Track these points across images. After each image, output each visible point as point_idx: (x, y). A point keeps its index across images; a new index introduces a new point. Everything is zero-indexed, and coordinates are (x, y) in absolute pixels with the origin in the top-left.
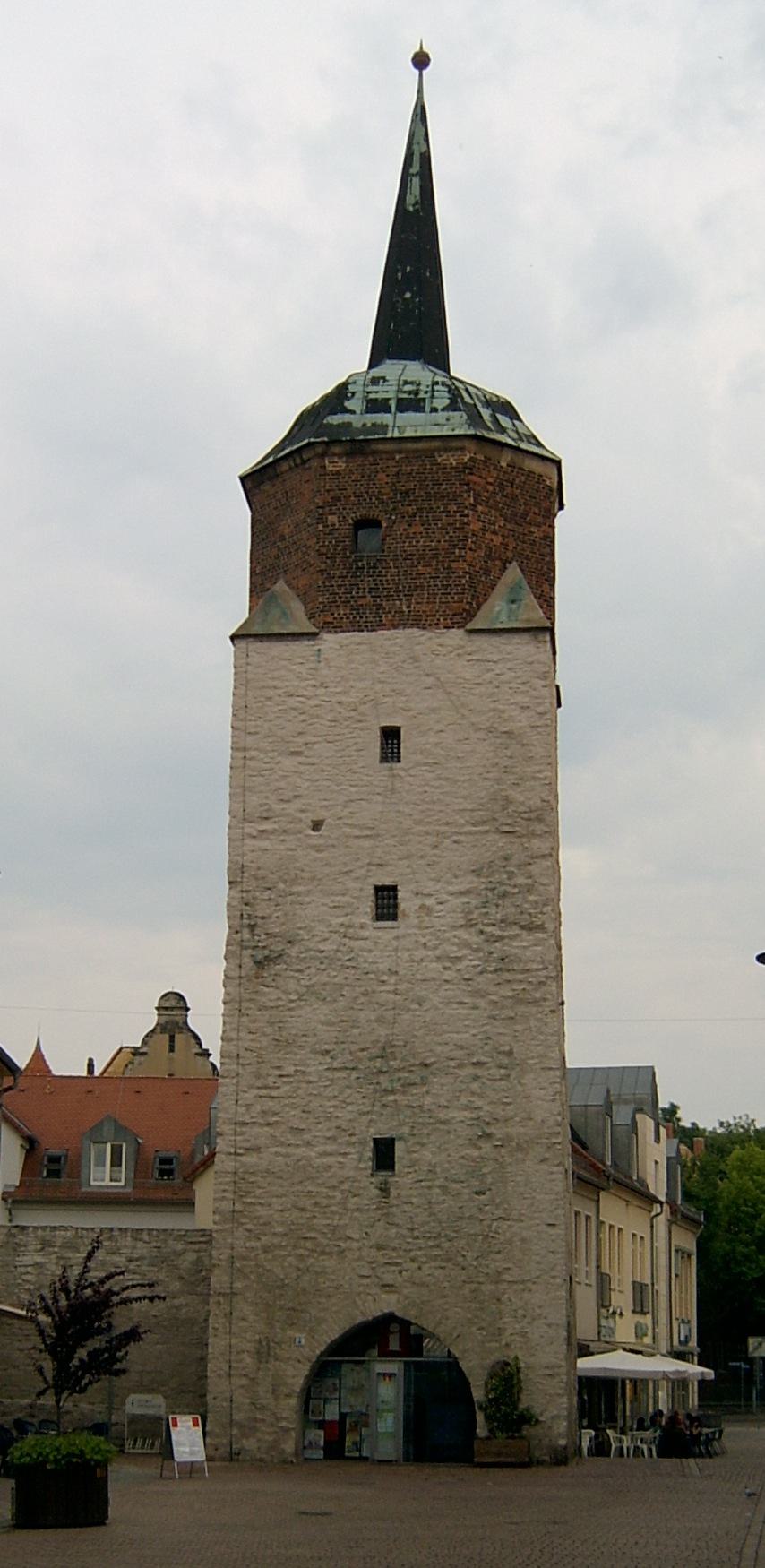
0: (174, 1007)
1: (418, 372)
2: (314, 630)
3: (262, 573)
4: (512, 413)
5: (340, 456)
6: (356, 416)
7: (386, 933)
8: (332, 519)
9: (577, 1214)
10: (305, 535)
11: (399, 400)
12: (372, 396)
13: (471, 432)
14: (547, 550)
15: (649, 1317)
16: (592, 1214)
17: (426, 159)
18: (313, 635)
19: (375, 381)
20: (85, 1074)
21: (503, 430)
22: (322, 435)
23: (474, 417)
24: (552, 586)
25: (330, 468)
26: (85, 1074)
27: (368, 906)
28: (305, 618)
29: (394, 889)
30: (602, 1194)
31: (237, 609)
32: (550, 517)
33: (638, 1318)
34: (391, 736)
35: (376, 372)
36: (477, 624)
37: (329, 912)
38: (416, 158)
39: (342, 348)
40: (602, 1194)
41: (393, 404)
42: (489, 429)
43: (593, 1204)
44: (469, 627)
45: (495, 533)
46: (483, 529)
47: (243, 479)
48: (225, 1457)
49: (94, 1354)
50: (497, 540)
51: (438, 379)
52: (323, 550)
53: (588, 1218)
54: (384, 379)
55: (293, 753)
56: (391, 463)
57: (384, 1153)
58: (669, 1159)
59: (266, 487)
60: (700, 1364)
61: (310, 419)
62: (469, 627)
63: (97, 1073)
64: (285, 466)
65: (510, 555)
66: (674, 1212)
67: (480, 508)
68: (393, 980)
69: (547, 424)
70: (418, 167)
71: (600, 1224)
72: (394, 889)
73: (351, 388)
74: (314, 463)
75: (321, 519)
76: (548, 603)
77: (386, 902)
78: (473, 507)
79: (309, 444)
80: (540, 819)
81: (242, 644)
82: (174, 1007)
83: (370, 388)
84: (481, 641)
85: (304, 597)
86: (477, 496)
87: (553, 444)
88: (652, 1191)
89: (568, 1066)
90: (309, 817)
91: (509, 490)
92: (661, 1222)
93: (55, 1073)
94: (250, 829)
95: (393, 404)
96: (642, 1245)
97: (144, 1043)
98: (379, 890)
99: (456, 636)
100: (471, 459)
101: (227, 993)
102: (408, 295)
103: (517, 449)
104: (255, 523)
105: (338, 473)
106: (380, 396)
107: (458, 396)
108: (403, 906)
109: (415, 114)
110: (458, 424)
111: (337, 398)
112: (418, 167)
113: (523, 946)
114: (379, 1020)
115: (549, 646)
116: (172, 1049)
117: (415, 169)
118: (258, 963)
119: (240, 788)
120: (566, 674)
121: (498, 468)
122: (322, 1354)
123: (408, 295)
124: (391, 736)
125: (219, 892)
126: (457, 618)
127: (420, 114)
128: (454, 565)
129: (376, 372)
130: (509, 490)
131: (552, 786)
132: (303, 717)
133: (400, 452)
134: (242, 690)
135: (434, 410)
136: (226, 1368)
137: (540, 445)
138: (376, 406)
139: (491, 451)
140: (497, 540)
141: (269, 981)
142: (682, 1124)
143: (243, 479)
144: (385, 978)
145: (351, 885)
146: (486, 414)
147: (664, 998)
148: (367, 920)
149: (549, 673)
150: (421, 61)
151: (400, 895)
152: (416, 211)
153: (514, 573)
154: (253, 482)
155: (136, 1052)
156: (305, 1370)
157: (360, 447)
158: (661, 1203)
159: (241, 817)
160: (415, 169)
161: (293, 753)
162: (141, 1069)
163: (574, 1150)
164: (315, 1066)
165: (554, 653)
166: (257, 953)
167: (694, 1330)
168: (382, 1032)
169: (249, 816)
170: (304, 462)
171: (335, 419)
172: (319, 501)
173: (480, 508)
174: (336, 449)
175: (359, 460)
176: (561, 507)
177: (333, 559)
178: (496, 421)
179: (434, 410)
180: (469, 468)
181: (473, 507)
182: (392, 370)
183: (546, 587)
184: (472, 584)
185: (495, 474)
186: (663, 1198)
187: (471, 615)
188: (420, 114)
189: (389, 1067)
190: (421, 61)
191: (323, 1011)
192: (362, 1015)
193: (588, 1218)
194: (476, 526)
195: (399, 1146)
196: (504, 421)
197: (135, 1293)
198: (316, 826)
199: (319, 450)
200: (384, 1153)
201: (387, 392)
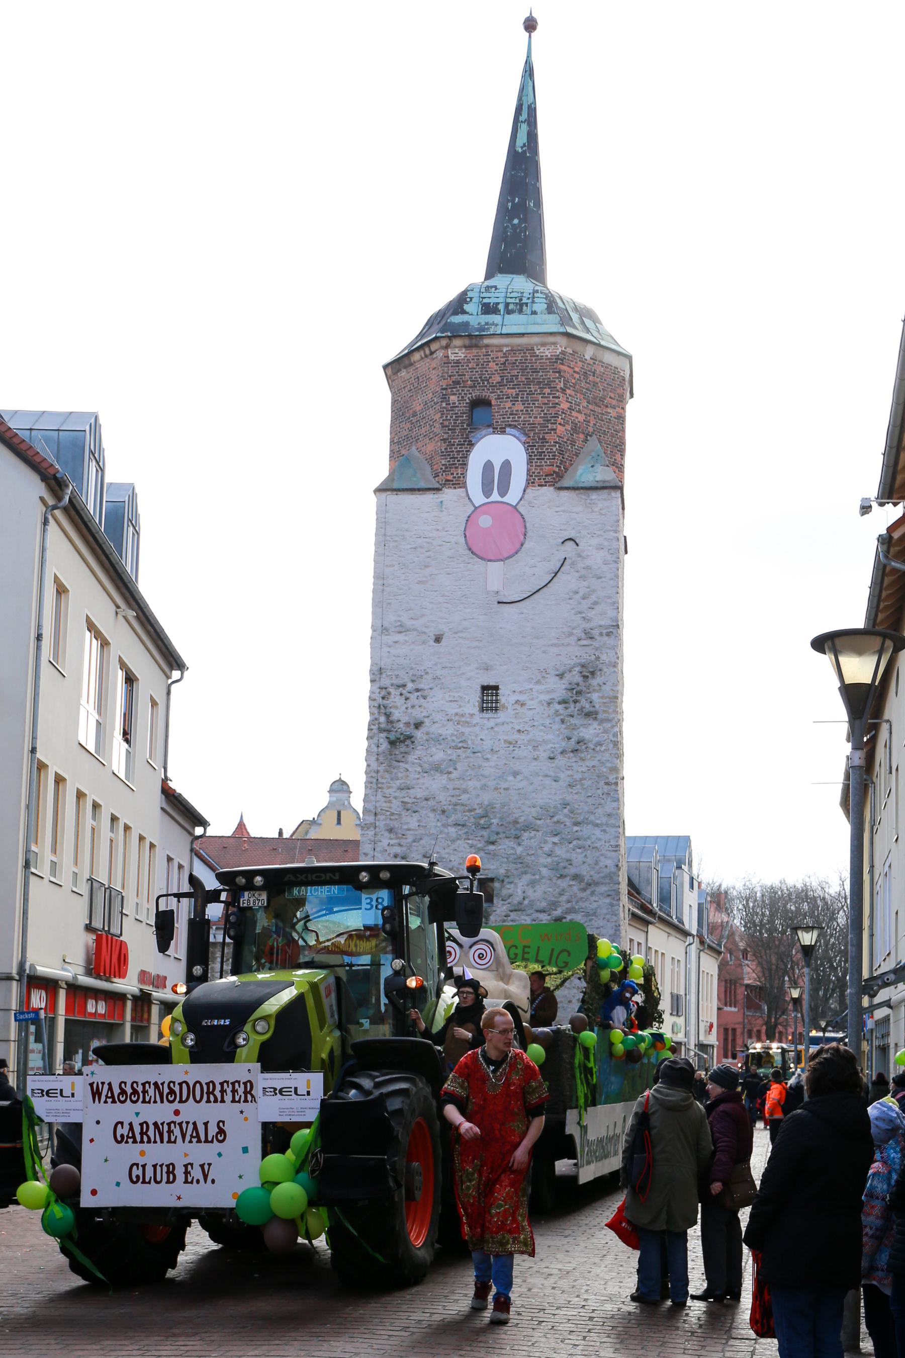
0: (340, 787)
1: (521, 284)
2: (437, 486)
3: (399, 443)
4: (595, 320)
5: (460, 347)
6: (473, 317)
8: (453, 398)
10: (432, 411)
11: (507, 305)
12: (485, 301)
13: (562, 330)
15: (682, 1019)
16: (643, 941)
17: (532, 111)
18: (438, 490)
19: (488, 288)
20: (277, 836)
21: (588, 330)
22: (449, 326)
24: (623, 456)
25: (452, 357)
26: (277, 836)
27: (475, 696)
28: (431, 478)
29: (496, 688)
31: (381, 470)
32: (621, 401)
33: (675, 1019)
34: (490, 691)
35: (489, 283)
36: (566, 483)
37: (447, 705)
39: (464, 263)
40: (650, 926)
42: (575, 327)
43: (644, 934)
44: (557, 485)
45: (579, 412)
47: (385, 367)
49: (394, 919)
50: (581, 418)
51: (539, 288)
52: (446, 423)
53: (639, 944)
56: (500, 354)
59: (403, 373)
60: (21, 1138)
62: (557, 485)
64: (417, 356)
65: (591, 429)
66: (702, 942)
70: (526, 115)
72: (496, 688)
73: (470, 294)
74: (440, 354)
75: (444, 398)
76: (619, 468)
78: (563, 391)
79: (436, 338)
80: (609, 634)
81: (383, 495)
82: (340, 787)
86: (566, 382)
87: (626, 344)
90: (432, 632)
91: (591, 378)
93: (253, 834)
95: (501, 307)
96: (679, 966)
97: (319, 815)
98: (484, 688)
99: (548, 491)
100: (563, 353)
101: (368, 766)
102: (516, 221)
103: (599, 345)
104: (394, 402)
105: (458, 362)
106: (492, 301)
107: (552, 305)
108: (503, 699)
110: (551, 324)
111: (459, 304)
112: (526, 115)
113: (591, 731)
114: (484, 787)
115: (620, 500)
116: (339, 822)
117: (524, 116)
118: (392, 743)
119: (381, 602)
120: (631, 527)
121: (583, 361)
124: (490, 691)
126: (549, 478)
127: (529, 71)
128: (547, 437)
129: (489, 283)
130: (591, 378)
131: (617, 606)
134: (396, 448)
135: (534, 313)
137: (619, 345)
138: (488, 309)
139: (578, 346)
140: (581, 418)
141: (400, 757)
143: (687, 839)
146: (575, 317)
148: (476, 710)
149: (617, 525)
150: (530, 25)
152: (524, 152)
153: (594, 444)
154: (394, 368)
155: (313, 822)
157: (473, 339)
158: (694, 936)
159: (380, 630)
160: (524, 116)
162: (314, 834)
163: (629, 893)
164: (432, 821)
165: (623, 508)
166: (393, 739)
167: (806, 992)
168: (486, 798)
170: (432, 353)
171: (458, 319)
173: (568, 392)
176: (632, 396)
177: (453, 430)
178: (583, 323)
179: (534, 313)
180: (559, 359)
181: (563, 391)
182: (501, 281)
183: (618, 456)
184: (561, 452)
185: (580, 364)
186: (694, 932)
187: (560, 476)
188: (529, 71)
190: (530, 25)
191: (442, 780)
193: (639, 944)
194: (565, 406)
195: (460, 491)
196: (588, 322)
198: (438, 640)
199: (444, 342)
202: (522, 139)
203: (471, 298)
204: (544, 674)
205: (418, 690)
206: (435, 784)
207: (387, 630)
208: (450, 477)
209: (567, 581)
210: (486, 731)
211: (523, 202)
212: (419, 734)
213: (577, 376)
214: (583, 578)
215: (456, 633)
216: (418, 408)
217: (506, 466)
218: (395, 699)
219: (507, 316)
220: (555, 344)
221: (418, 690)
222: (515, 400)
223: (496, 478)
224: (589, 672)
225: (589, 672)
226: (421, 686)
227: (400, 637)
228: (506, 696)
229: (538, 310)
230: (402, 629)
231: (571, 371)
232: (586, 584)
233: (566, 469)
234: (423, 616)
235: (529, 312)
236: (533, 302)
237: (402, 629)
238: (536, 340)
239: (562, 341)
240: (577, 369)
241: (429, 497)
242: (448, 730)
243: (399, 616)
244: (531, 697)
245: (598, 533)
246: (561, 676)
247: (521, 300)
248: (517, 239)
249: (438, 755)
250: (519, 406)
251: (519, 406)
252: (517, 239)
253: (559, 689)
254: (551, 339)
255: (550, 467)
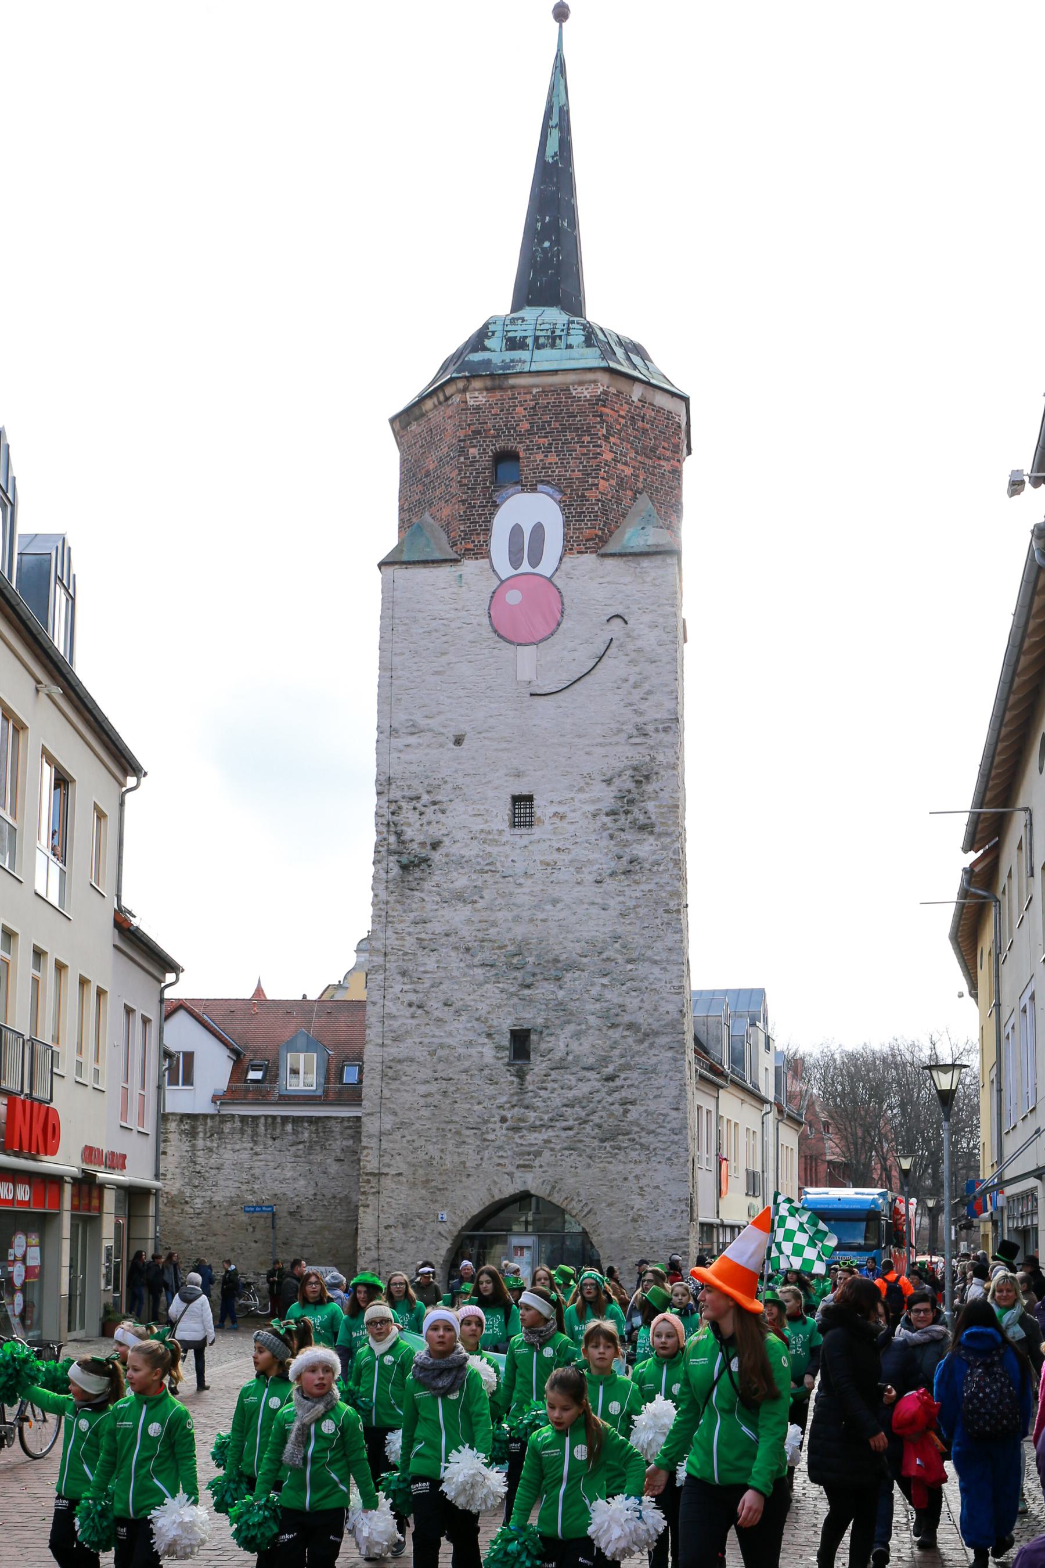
1: (555, 316)
2: (455, 556)
3: (410, 509)
5: (480, 390)
6: (496, 353)
7: (522, 837)
8: (473, 451)
9: (747, 1129)
10: (448, 469)
11: (537, 338)
12: (510, 335)
13: (603, 364)
14: (803, 1147)
16: (713, 1109)
17: (564, 115)
18: (456, 561)
21: (635, 367)
23: (607, 352)
27: (504, 809)
28: (448, 547)
30: (721, 1091)
31: (387, 537)
34: (522, 802)
35: (514, 315)
36: (611, 548)
37: (471, 821)
38: (556, 111)
39: (489, 288)
40: (721, 1091)
41: (530, 341)
43: (713, 1101)
45: (626, 464)
46: (615, 460)
47: (762, 992)
48: (545, 251)
50: (628, 471)
52: (465, 481)
53: (708, 1112)
54: (523, 320)
55: (436, 673)
56: (529, 397)
57: (521, 1043)
58: (776, 1068)
61: (457, 360)
63: (698, 1466)
65: (640, 485)
66: (780, 1111)
67: (612, 439)
68: (529, 882)
69: (671, 363)
70: (557, 121)
71: (719, 1118)
73: (491, 328)
74: (457, 399)
75: (462, 451)
77: (522, 804)
81: (390, 570)
83: (509, 328)
84: (609, 562)
85: (447, 527)
86: (609, 427)
88: (763, 1094)
89: (692, 989)
90: (451, 732)
91: (640, 424)
92: (771, 1118)
94: (399, 742)
95: (530, 341)
98: (516, 799)
99: (590, 559)
100: (605, 393)
101: (376, 896)
102: (547, 244)
103: (649, 384)
104: (403, 462)
105: (478, 408)
106: (519, 334)
107: (590, 336)
108: (538, 812)
109: (555, 67)
110: (591, 358)
112: (557, 121)
113: (645, 848)
114: (517, 919)
118: (404, 868)
122: (463, 1229)
123: (547, 244)
124: (522, 802)
125: (369, 802)
126: (591, 544)
127: (560, 67)
128: (587, 493)
130: (640, 424)
131: (675, 696)
132: (445, 639)
133: (537, 386)
135: (569, 347)
136: (374, 1240)
138: (514, 344)
139: (623, 385)
140: (628, 471)
141: (414, 885)
142: (444, 1488)
143: (762, 992)
144: (521, 881)
145: (490, 794)
146: (619, 352)
147: (820, 919)
148: (505, 826)
150: (561, 13)
151: (535, 802)
152: (556, 163)
154: (404, 421)
156: (446, 1245)
157: (497, 379)
161: (436, 673)
162: (340, 996)
164: (455, 961)
168: (519, 931)
169: (398, 725)
170: (447, 399)
172: (461, 434)
173: (612, 439)
174: (477, 384)
175: (498, 394)
177: (473, 489)
178: (629, 359)
179: (569, 347)
180: (602, 400)
181: (606, 438)
182: (530, 313)
184: (605, 512)
185: (626, 407)
186: (772, 1100)
187: (603, 541)
188: (560, 67)
189: (523, 965)
190: (561, 13)
192: (500, 914)
193: (708, 1112)
194: (608, 456)
197: (6, 1558)
198: (458, 741)
199: (461, 384)
200: (521, 1043)
201: (523, 331)
202: (553, 146)
203: (493, 333)
204: (588, 780)
205: (434, 803)
206: (458, 916)
207: (396, 731)
208: (471, 546)
209: (614, 667)
210: (517, 850)
211: (555, 221)
212: (437, 856)
213: (623, 421)
214: (633, 662)
215: (480, 733)
216: (431, 467)
217: (538, 530)
218: (407, 815)
219: (536, 352)
220: (595, 382)
221: (434, 803)
222: (547, 451)
223: (527, 545)
224: (642, 776)
225: (642, 776)
226: (439, 798)
227: (412, 740)
228: (542, 808)
229: (574, 344)
230: (415, 730)
231: (615, 415)
232: (637, 669)
233: (611, 533)
234: (439, 713)
235: (563, 346)
236: (568, 334)
237: (415, 730)
238: (571, 378)
239: (604, 378)
240: (622, 413)
241: (444, 572)
242: (471, 851)
243: (410, 714)
244: (573, 813)
245: (651, 608)
246: (609, 782)
247: (553, 332)
248: (550, 267)
249: (461, 881)
250: (553, 458)
251: (553, 458)
252: (550, 267)
253: (607, 796)
254: (590, 376)
255: (593, 530)
